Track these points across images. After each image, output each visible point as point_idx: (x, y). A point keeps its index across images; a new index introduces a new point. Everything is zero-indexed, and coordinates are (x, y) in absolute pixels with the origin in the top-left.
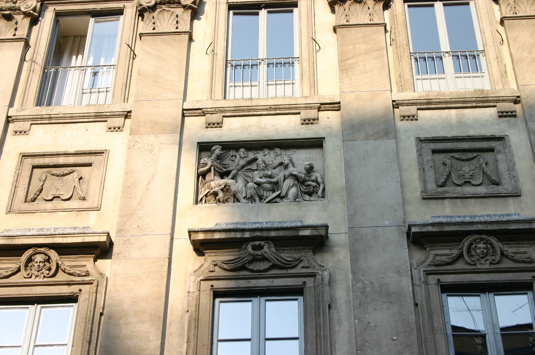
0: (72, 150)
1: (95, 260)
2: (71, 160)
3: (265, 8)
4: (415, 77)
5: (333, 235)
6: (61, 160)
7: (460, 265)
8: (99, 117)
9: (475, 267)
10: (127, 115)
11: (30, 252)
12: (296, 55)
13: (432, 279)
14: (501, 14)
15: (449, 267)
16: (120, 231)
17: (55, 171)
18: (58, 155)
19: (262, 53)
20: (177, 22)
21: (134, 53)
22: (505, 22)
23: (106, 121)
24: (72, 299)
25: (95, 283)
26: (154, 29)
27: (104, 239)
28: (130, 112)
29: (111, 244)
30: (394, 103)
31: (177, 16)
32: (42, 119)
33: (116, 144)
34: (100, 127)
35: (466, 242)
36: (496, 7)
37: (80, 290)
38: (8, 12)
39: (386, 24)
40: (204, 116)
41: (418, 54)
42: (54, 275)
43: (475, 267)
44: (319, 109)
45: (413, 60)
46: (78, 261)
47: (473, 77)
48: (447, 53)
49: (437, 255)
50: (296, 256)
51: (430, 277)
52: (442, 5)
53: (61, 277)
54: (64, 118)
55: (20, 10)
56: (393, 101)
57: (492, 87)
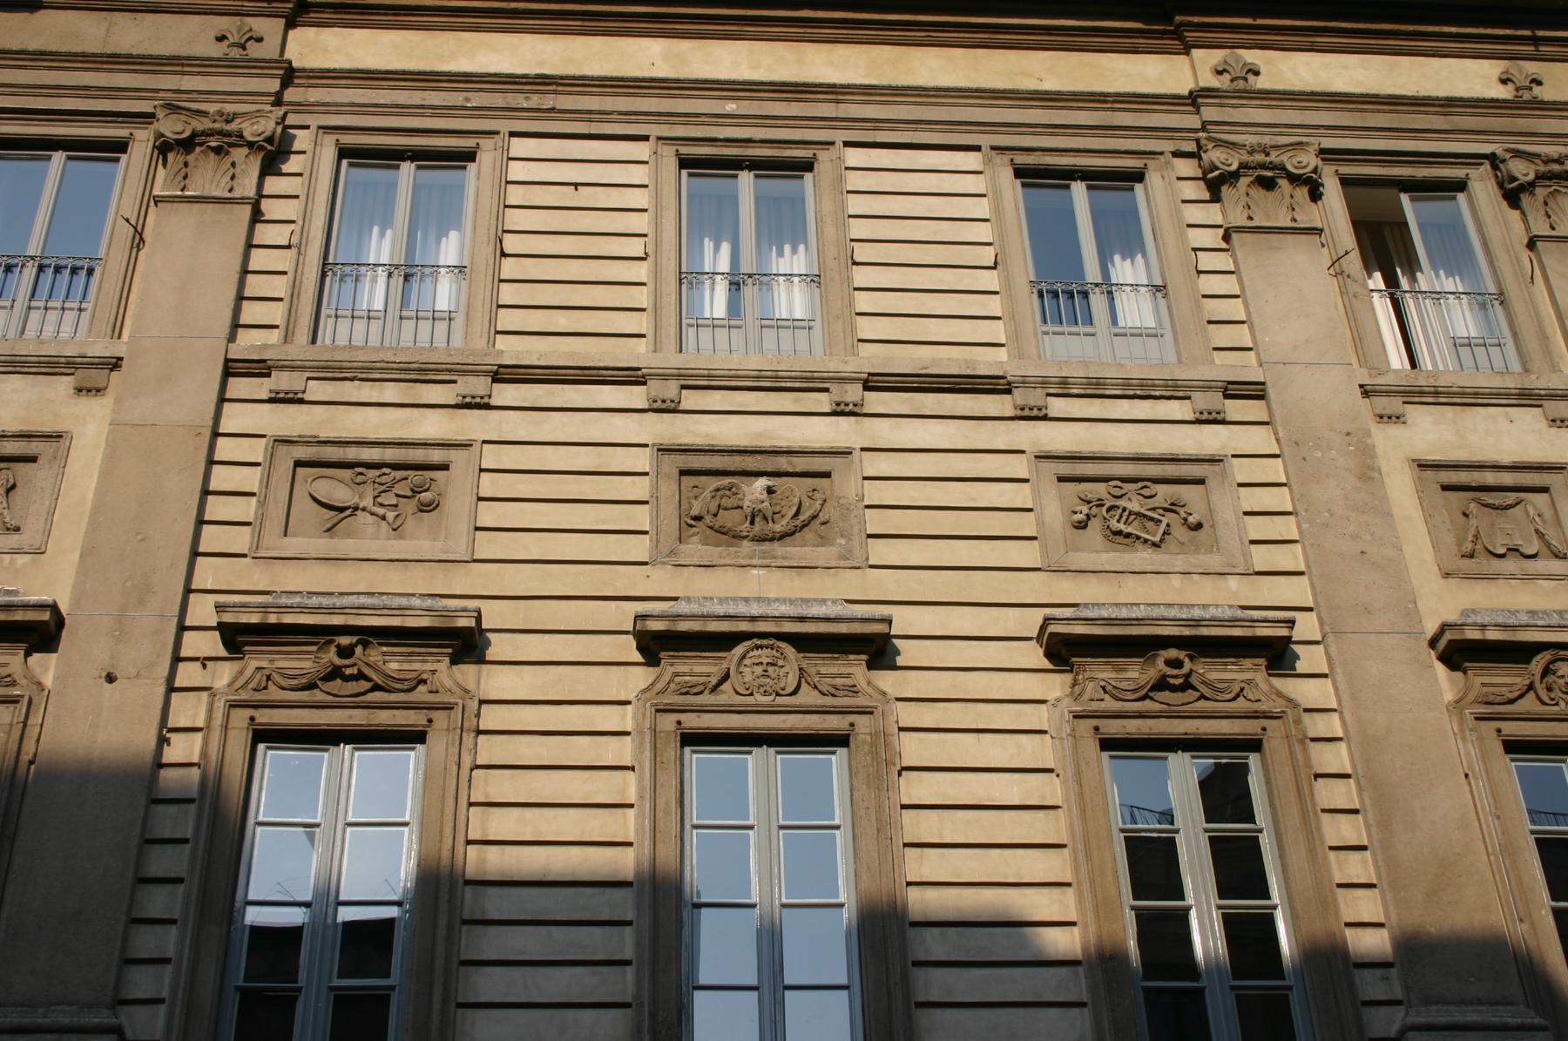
0: (1506, 460)
1: (28, 654)
2: (1508, 479)
3: (750, 168)
4: (684, 321)
6: (1490, 478)
7: (1528, 704)
8: (51, 367)
9: (750, 700)
10: (115, 364)
13: (241, 717)
15: (707, 699)
16: (77, 600)
18: (1481, 467)
20: (233, 178)
21: (141, 238)
22: (1234, 236)
23: (455, 382)
24: (414, 737)
25: (26, 701)
26: (230, 191)
27: (46, 616)
28: (121, 359)
31: (233, 165)
32: (1422, 393)
33: (89, 424)
35: (739, 650)
36: (1515, 215)
37: (430, 721)
38: (1270, 174)
43: (750, 700)
45: (1035, 295)
46: (1225, 671)
48: (750, 276)
49: (677, 674)
54: (1463, 394)
55: (241, 136)
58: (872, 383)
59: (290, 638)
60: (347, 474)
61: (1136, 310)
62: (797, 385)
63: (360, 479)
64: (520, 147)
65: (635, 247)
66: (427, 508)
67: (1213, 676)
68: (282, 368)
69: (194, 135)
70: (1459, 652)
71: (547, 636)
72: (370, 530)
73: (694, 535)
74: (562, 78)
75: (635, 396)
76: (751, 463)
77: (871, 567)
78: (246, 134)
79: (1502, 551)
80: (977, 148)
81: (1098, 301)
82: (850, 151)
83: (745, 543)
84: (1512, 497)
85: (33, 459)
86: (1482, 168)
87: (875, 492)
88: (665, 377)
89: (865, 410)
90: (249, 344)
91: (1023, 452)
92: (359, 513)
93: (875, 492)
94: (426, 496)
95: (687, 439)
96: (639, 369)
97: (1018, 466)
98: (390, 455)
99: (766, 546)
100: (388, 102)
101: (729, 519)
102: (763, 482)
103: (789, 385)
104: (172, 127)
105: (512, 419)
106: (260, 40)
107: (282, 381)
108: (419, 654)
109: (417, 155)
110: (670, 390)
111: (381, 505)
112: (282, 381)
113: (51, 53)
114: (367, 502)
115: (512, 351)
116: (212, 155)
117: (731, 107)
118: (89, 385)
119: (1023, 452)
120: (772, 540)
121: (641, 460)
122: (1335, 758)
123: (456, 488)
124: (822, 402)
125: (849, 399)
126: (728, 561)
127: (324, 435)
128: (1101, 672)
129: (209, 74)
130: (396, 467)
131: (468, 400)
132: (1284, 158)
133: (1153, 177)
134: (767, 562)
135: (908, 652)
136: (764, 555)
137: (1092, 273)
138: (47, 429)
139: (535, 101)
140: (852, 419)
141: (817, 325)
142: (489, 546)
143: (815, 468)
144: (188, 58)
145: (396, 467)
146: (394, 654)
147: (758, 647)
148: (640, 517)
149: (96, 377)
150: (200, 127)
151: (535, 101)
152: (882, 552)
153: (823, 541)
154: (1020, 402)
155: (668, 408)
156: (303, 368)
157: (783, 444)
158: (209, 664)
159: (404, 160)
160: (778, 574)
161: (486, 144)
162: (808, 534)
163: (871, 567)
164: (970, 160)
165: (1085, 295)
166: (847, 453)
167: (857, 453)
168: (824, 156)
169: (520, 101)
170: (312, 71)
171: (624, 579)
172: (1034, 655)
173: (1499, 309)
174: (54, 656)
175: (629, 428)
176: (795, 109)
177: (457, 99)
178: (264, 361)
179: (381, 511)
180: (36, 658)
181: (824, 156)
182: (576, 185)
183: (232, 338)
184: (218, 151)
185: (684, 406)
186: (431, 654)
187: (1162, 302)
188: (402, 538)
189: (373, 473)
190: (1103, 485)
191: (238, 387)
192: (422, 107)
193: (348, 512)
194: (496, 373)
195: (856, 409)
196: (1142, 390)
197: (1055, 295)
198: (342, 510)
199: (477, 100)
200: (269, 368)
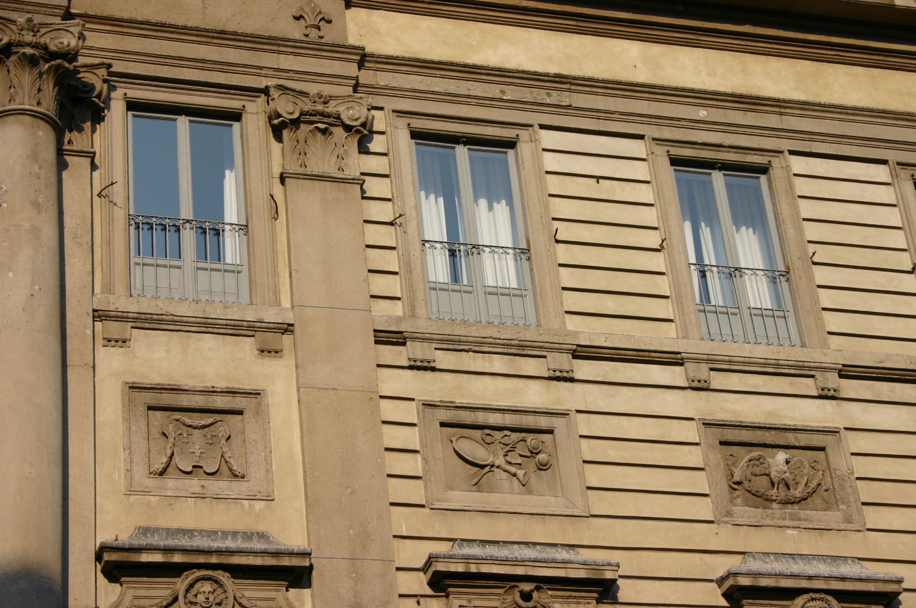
4: (133, 260)
5: (325, 561)
8: (236, 329)
23: (545, 357)
30: (96, 314)
33: (278, 380)
36: (276, 147)
39: (94, 153)
40: (404, 344)
41: (207, 224)
45: (132, 228)
47: (212, 270)
48: (188, 221)
52: (187, 122)
56: (94, 311)
57: (404, 313)
58: (847, 372)
59: (483, 583)
60: (477, 434)
62: (792, 372)
63: (489, 439)
65: (652, 239)
66: (543, 467)
67: (247, 594)
68: (415, 339)
71: (657, 583)
72: (506, 485)
73: (738, 497)
74: (575, 78)
76: (769, 437)
77: (869, 530)
78: (343, 117)
79: (189, 469)
80: (884, 162)
82: (794, 159)
83: (775, 505)
84: (208, 419)
86: (259, 100)
87: (865, 467)
88: (697, 361)
89: (842, 396)
91: (413, 400)
92: (494, 469)
93: (865, 467)
94: (542, 457)
95: (720, 416)
96: (679, 353)
98: (509, 420)
99: (789, 510)
100: (409, 86)
101: (761, 484)
102: (781, 456)
103: (786, 371)
104: (287, 108)
105: (590, 394)
106: (329, 22)
107: (416, 350)
108: (575, 597)
109: (725, 167)
110: (702, 372)
111: (510, 463)
112: (416, 350)
113: (170, 26)
114: (500, 461)
116: (319, 135)
117: (702, 114)
118: (268, 347)
119: (413, 400)
120: (793, 503)
121: (690, 432)
123: (567, 450)
124: (807, 386)
125: (831, 386)
126: (767, 522)
127: (459, 400)
129: (300, 55)
130: (514, 430)
131: (558, 374)
132: (341, 109)
133: (524, 148)
134: (796, 523)
136: (793, 517)
138: (247, 387)
139: (554, 98)
140: (834, 402)
142: (601, 503)
143: (812, 444)
144: (283, 39)
145: (514, 430)
146: (557, 597)
147: (813, 599)
148: (699, 482)
149: (271, 339)
150: (306, 108)
151: (554, 98)
152: (875, 517)
153: (828, 506)
154: (691, 375)
155: (701, 387)
156: (430, 340)
157: (790, 423)
158: (422, 600)
159: (458, 143)
160: (806, 534)
161: (524, 134)
162: (816, 500)
163: (869, 530)
164: (880, 173)
165: (217, 233)
166: (835, 432)
167: (573, 414)
168: (776, 162)
169: (541, 96)
170: (379, 56)
171: (701, 537)
173: (785, 285)
174: (307, 592)
175: (667, 400)
176: (749, 119)
177: (493, 91)
178: (401, 332)
179: (513, 469)
181: (776, 162)
182: (598, 178)
184: (324, 132)
185: (713, 385)
186: (583, 597)
187: (526, 264)
188: (530, 492)
189: (498, 435)
190: (479, 432)
192: (469, 97)
193: (487, 469)
194: (575, 351)
195: (836, 394)
196: (775, 370)
198: (482, 467)
199: (512, 93)
200: (405, 338)
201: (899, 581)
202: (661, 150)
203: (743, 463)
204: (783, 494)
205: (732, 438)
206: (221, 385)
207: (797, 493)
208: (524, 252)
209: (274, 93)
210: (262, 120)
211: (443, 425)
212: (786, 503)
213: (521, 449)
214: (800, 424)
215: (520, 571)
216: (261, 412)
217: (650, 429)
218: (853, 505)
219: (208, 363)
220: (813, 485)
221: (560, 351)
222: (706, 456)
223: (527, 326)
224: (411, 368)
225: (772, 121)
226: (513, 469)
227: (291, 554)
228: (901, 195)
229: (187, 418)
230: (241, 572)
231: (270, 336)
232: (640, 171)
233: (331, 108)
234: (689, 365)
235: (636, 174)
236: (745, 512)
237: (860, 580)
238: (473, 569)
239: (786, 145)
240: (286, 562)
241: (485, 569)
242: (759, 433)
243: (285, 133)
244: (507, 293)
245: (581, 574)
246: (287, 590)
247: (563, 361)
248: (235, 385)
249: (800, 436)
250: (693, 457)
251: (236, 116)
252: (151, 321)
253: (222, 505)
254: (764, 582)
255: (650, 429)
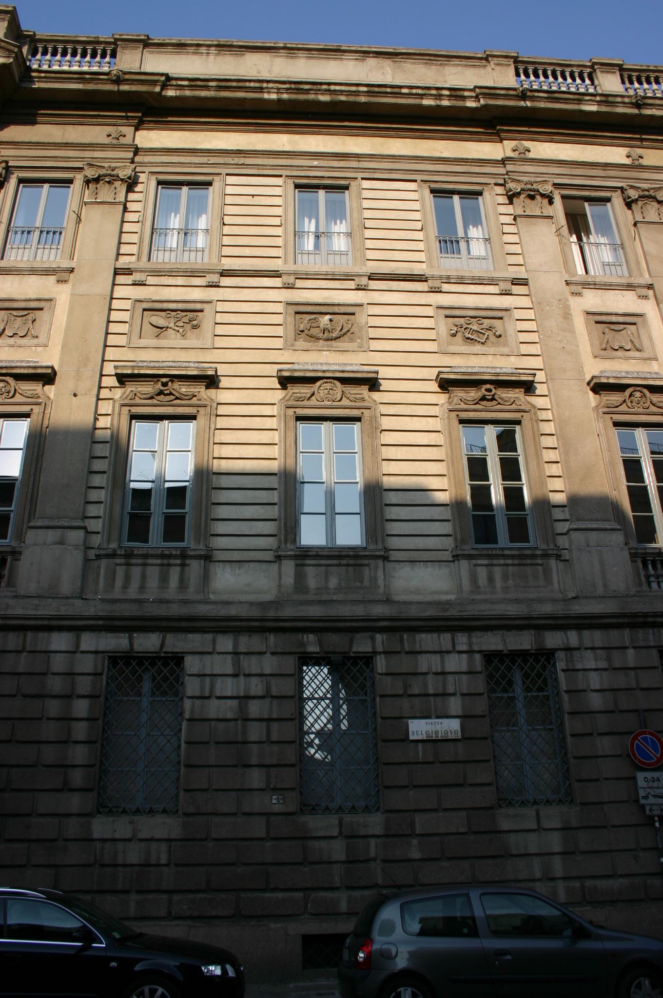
0: (621, 312)
1: (43, 386)
2: (621, 319)
6: (614, 319)
7: (623, 408)
10: (72, 270)
11: (631, 389)
12: (65, 226)
14: (634, 218)
16: (61, 365)
17: (613, 327)
19: (38, 224)
27: (49, 371)
29: (55, 373)
32: (589, 284)
33: (63, 294)
34: (630, 295)
35: (318, 383)
42: (13, 397)
44: (370, 279)
50: (197, 390)
51: (123, 408)
53: (18, 398)
60: (163, 314)
61: (478, 249)
64: (230, 180)
65: (277, 221)
66: (195, 327)
69: (99, 176)
70: (598, 388)
72: (173, 336)
75: (277, 282)
80: (415, 181)
81: (463, 245)
84: (622, 326)
85: (42, 309)
87: (373, 321)
88: (289, 274)
90: (123, 262)
93: (373, 321)
94: (195, 323)
97: (429, 311)
99: (329, 343)
101: (314, 331)
102: (328, 317)
104: (91, 173)
105: (228, 292)
106: (124, 136)
107: (137, 277)
112: (137, 277)
114: (172, 325)
115: (228, 264)
117: (315, 163)
121: (280, 308)
122: (549, 428)
123: (207, 319)
124: (352, 285)
127: (154, 298)
128: (459, 393)
135: (384, 385)
137: (461, 233)
138: (47, 297)
141: (350, 253)
143: (349, 311)
149: (64, 276)
150: (102, 173)
152: (374, 345)
153: (352, 340)
154: (431, 285)
155: (290, 287)
161: (216, 178)
165: (458, 242)
168: (353, 184)
172: (434, 387)
177: (204, 160)
179: (177, 329)
180: (47, 387)
182: (253, 196)
183: (117, 259)
184: (109, 182)
187: (488, 246)
188: (185, 339)
189: (174, 314)
191: (120, 279)
197: (446, 241)
198: (162, 328)
199: (213, 160)
201: (377, 373)
202: (290, 182)
203: (306, 321)
204: (326, 335)
205: (301, 310)
206: (34, 297)
207: (334, 335)
208: (487, 240)
209: (86, 168)
210: (621, 200)
211: (446, 317)
212: (327, 340)
213: (186, 320)
214: (341, 302)
215: (161, 372)
216: (645, 323)
217: (257, 307)
218: (365, 340)
219: (622, 302)
220: (344, 331)
221: (213, 273)
222: (285, 319)
223: (196, 263)
224: (133, 285)
225: (354, 164)
226: (177, 329)
227: (42, 367)
228: (422, 196)
229: (15, 313)
230: (19, 377)
231: (63, 274)
232: (278, 191)
233: (535, 186)
234: (284, 277)
235: (276, 193)
236: (301, 344)
237: (353, 372)
238: (136, 372)
239: (360, 175)
240: (39, 371)
241: (142, 372)
242: (318, 307)
243: (90, 185)
244: (341, 253)
245: (195, 373)
246: (43, 386)
247: (215, 278)
248: (41, 297)
249: (341, 308)
250: (279, 319)
251: (608, 200)
252: (6, 270)
253: (22, 350)
254: (296, 374)
255: (257, 307)
